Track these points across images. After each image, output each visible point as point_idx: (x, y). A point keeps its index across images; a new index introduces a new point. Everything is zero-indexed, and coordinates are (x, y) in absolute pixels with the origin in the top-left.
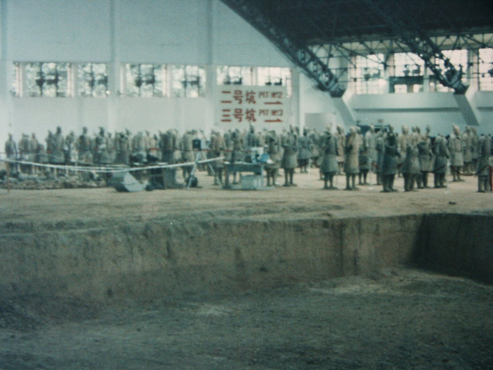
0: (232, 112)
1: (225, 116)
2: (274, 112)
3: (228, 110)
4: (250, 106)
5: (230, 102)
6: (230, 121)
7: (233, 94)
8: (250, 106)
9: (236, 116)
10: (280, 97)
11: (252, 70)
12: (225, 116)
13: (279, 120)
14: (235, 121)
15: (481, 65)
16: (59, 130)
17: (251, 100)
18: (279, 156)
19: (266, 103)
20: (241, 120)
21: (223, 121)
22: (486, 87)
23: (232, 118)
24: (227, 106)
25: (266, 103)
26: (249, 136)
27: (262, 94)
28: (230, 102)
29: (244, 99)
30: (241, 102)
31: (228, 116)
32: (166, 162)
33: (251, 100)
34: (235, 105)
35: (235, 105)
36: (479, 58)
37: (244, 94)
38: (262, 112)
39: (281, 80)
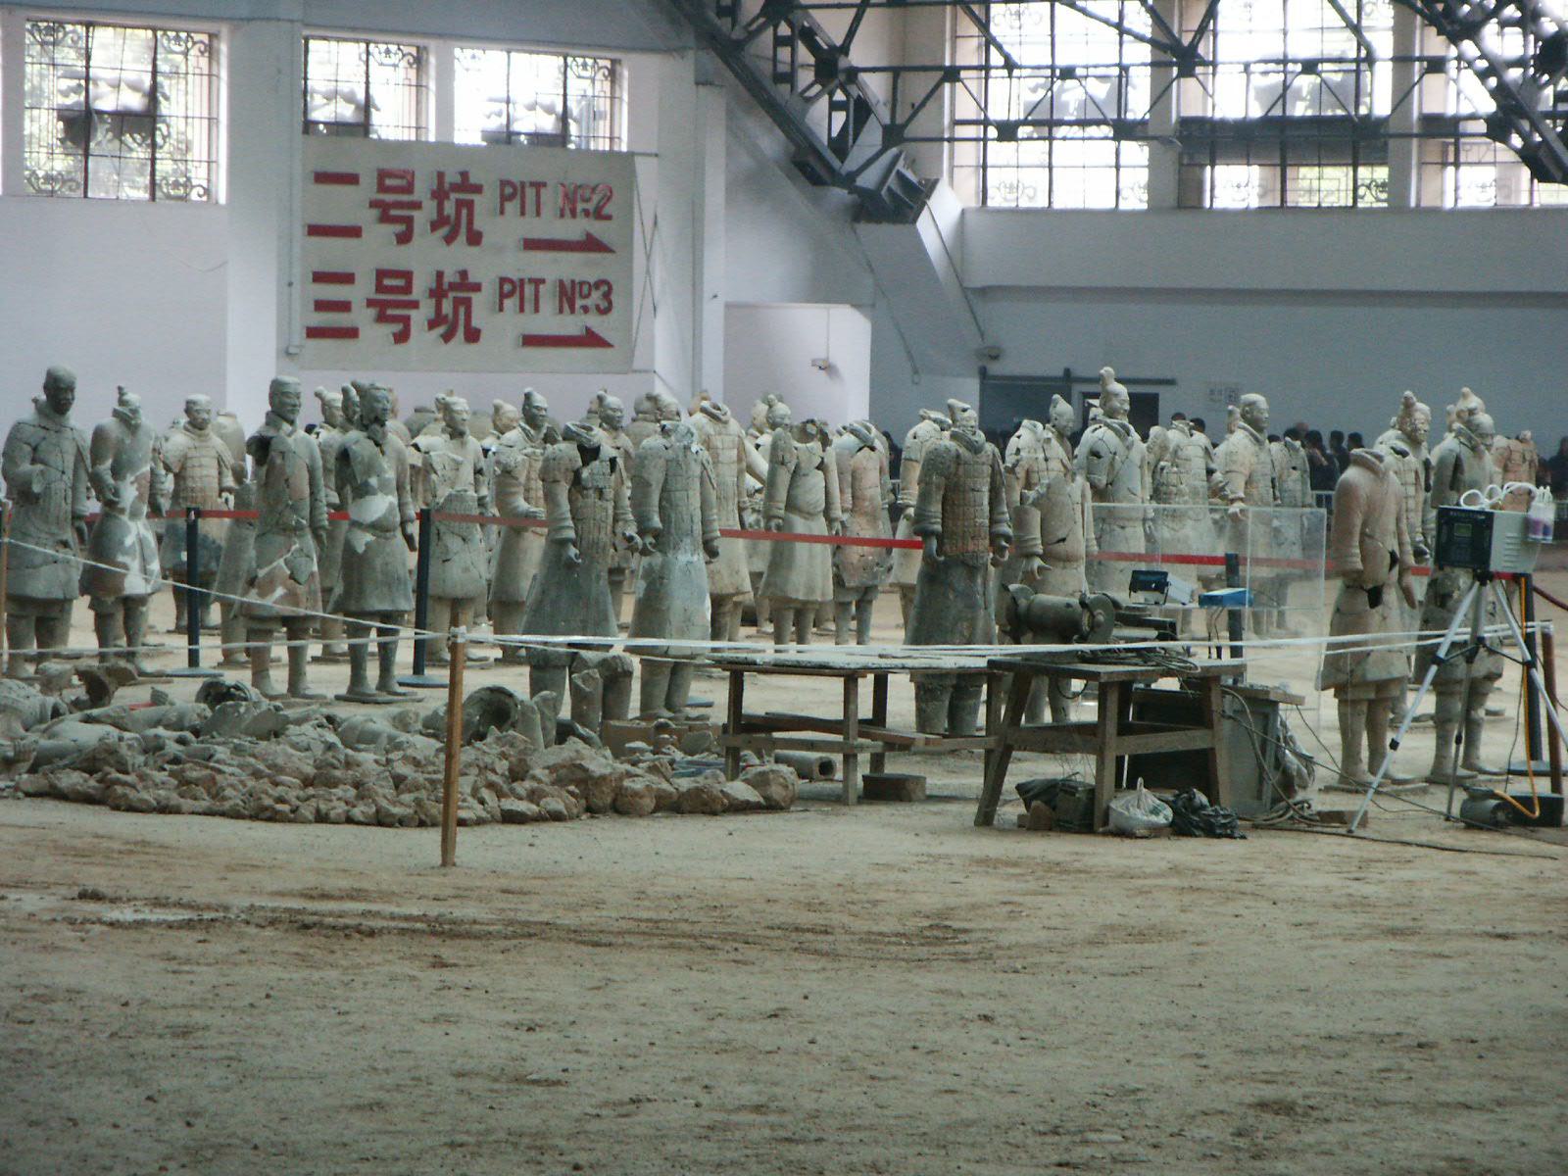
0: (360, 292)
1: (321, 306)
2: (569, 295)
3: (347, 278)
4: (456, 258)
5: (354, 232)
6: (351, 333)
7: (367, 188)
8: (456, 258)
9: (383, 312)
10: (599, 214)
11: (419, 62)
12: (321, 306)
13: (591, 340)
14: (375, 335)
15: (999, 82)
16: (35, 401)
17: (459, 226)
18: (1488, 643)
19: (531, 245)
20: (402, 337)
21: (313, 333)
22: (1015, 188)
23: (361, 316)
24: (335, 253)
25: (531, 245)
26: (1209, 488)
27: (511, 192)
28: (354, 232)
29: (421, 219)
30: (404, 238)
31: (344, 306)
32: (1210, 689)
33: (459, 226)
34: (376, 249)
35: (376, 249)
36: (990, 41)
37: (422, 191)
38: (510, 289)
39: (564, 118)
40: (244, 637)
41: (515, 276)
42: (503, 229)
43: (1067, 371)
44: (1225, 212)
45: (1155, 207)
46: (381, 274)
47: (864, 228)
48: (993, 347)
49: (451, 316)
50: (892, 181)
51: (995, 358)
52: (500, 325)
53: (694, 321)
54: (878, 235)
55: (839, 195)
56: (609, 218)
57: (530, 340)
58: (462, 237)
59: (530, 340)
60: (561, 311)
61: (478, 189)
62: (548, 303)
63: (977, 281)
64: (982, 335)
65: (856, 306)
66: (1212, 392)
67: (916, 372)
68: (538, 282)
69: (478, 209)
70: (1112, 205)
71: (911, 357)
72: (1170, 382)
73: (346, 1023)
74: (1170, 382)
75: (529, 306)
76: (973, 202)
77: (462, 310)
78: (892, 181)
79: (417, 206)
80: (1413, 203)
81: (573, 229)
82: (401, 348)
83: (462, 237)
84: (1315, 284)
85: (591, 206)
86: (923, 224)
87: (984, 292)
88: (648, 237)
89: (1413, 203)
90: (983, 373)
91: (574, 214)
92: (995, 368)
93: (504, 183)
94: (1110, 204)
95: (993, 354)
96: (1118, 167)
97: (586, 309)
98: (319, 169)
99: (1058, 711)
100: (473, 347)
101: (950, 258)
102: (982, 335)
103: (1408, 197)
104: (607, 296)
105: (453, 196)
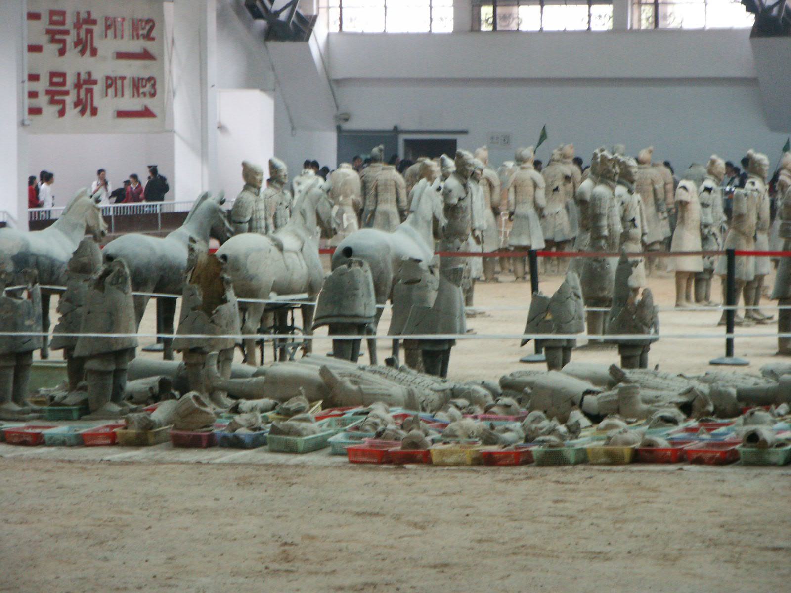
2: (137, 85)
10: (148, 37)
13: (146, 113)
19: (121, 56)
20: (62, 113)
25: (121, 56)
30: (62, 52)
40: (152, 288)
41: (112, 74)
42: (106, 45)
43: (396, 128)
44: (679, 32)
45: (457, 31)
46: (53, 74)
47: (273, 45)
48: (346, 114)
49: (84, 100)
50: (294, 18)
51: (346, 120)
52: (106, 104)
53: (202, 102)
54: (281, 49)
55: (261, 23)
56: (153, 39)
57: (121, 114)
58: (88, 52)
59: (121, 114)
60: (134, 96)
61: (94, 22)
62: (128, 91)
63: (338, 74)
64: (337, 107)
65: (263, 90)
66: (492, 138)
67: (293, 129)
68: (123, 78)
69: (95, 34)
70: (585, 27)
71: (291, 120)
72: (464, 132)
73: (513, 474)
74: (464, 132)
75: (119, 93)
76: (335, 29)
77: (89, 95)
78: (294, 18)
79: (67, 32)
80: (629, 27)
81: (136, 46)
82: (61, 119)
83: (88, 52)
84: (596, 74)
85: (145, 32)
86: (312, 41)
87: (338, 82)
88: (170, 50)
89: (629, 27)
90: (339, 129)
91: (138, 38)
92: (347, 126)
93: (107, 19)
94: (427, 30)
95: (346, 116)
96: (341, 7)
97: (145, 94)
98: (92, 12)
99: (44, 356)
100: (94, 118)
101: (323, 63)
102: (337, 107)
103: (626, 24)
104: (154, 86)
105: (85, 27)
